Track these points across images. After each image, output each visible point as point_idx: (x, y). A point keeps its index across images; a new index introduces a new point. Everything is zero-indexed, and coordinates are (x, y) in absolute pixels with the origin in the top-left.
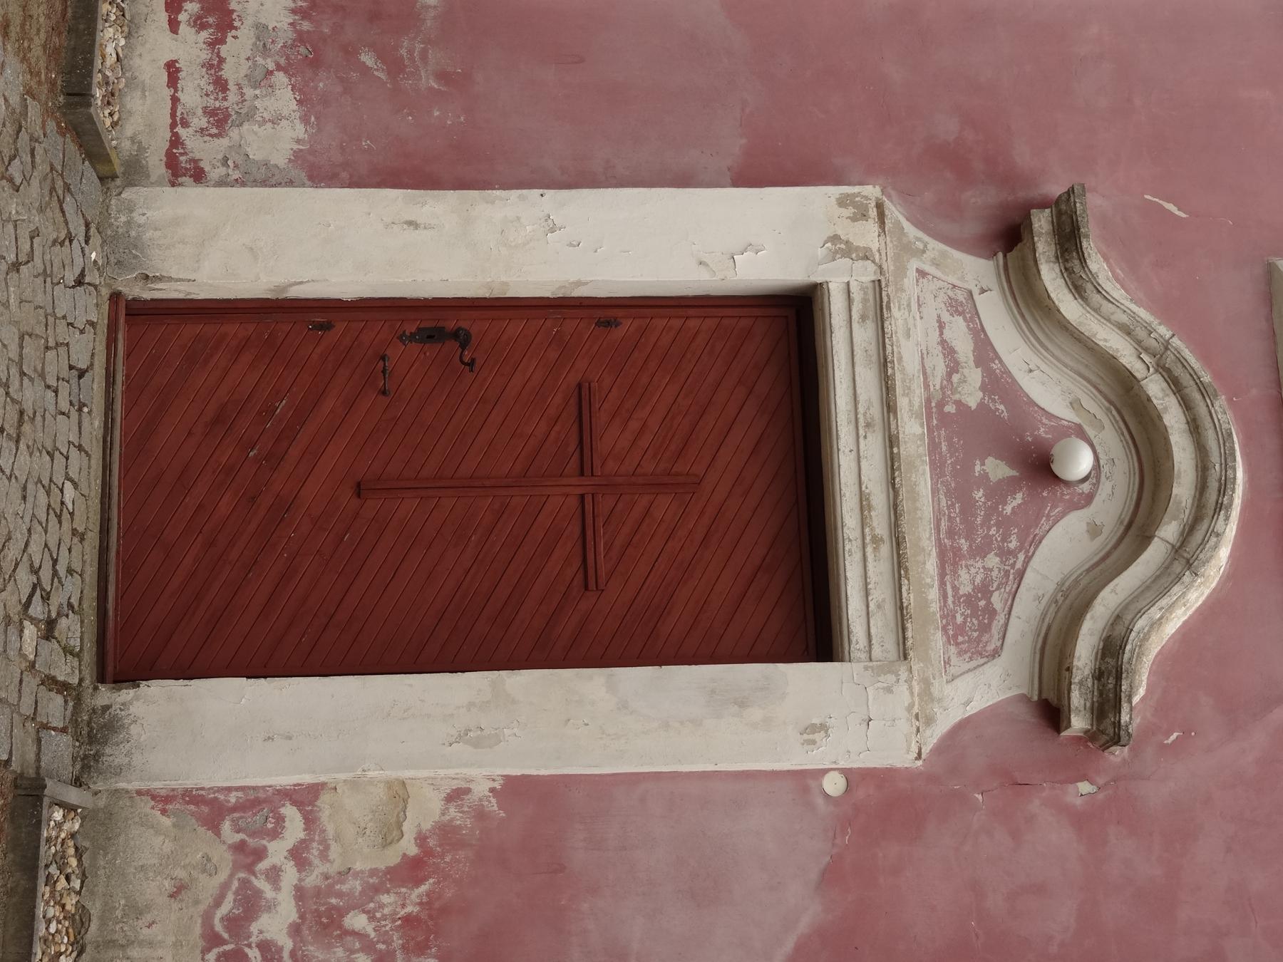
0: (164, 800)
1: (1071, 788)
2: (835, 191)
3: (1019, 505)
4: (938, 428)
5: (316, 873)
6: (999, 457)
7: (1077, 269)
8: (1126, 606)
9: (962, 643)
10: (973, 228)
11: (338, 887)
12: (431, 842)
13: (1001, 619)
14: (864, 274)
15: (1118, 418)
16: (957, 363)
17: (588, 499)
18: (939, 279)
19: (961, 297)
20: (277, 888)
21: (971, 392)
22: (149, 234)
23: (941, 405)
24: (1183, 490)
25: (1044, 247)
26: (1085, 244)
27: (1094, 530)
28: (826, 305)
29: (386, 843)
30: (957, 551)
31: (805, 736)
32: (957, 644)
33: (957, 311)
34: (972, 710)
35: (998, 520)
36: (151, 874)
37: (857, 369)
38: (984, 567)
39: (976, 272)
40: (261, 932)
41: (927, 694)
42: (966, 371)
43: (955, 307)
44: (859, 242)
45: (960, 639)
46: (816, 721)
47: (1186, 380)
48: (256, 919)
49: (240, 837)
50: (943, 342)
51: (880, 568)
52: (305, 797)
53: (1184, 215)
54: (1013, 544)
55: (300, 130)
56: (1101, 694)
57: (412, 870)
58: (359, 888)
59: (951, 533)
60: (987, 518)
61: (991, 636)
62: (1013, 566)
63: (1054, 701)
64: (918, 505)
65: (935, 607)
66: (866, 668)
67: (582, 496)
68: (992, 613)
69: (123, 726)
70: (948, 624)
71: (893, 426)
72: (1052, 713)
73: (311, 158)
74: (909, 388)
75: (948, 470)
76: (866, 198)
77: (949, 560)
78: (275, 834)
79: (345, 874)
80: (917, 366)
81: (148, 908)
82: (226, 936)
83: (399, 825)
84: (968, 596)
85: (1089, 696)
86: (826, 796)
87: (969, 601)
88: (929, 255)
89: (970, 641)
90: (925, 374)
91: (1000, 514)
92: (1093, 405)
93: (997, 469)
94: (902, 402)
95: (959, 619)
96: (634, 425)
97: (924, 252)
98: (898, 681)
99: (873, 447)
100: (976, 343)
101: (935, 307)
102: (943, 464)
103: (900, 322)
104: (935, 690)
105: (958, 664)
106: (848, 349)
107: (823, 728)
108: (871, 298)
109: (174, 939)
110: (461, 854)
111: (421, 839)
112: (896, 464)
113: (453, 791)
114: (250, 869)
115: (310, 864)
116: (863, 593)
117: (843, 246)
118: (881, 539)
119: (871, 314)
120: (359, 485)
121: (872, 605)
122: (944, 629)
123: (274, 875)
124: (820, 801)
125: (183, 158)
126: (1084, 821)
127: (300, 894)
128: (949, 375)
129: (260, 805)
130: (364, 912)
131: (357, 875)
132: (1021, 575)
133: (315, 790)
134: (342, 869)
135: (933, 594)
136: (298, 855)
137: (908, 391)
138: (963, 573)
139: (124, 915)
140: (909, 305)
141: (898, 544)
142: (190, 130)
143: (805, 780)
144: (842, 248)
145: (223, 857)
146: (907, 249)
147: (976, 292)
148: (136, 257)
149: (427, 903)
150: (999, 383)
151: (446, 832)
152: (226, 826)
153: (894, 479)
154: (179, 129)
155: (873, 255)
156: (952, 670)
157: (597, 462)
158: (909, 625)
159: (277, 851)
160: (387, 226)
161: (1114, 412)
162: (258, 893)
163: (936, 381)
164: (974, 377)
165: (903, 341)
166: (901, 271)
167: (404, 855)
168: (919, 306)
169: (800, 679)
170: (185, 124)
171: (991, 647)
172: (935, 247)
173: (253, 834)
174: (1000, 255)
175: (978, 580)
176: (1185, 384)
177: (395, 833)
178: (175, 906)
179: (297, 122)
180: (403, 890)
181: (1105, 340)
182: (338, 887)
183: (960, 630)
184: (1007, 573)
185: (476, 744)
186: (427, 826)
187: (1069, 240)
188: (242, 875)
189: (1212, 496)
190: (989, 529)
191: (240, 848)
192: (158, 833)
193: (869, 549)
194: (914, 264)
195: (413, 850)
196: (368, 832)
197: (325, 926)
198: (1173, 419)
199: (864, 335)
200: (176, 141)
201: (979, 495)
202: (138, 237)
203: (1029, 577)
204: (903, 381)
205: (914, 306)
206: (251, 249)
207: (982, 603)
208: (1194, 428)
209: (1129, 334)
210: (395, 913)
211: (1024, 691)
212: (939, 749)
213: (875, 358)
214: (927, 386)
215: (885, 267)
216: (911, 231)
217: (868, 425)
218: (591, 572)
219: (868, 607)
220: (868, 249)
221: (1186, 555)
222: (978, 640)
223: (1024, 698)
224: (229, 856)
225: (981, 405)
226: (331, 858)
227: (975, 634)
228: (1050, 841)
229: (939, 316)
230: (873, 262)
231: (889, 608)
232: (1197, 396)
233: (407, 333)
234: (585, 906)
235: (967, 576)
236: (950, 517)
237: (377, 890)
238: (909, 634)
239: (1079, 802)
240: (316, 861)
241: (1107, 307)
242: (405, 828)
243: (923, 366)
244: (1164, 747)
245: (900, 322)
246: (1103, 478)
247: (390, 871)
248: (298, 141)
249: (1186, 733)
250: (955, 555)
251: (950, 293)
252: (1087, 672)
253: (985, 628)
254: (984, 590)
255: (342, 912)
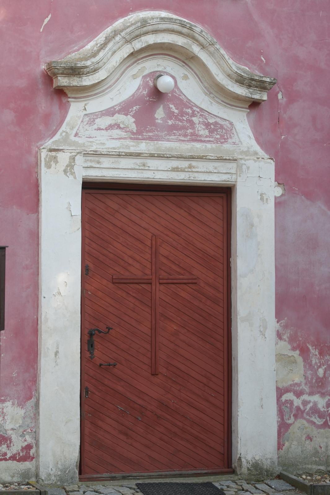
0: (280, 446)
1: (280, 101)
2: (43, 169)
3: (174, 106)
4: (143, 135)
5: (305, 388)
6: (154, 112)
7: (88, 70)
8: (224, 71)
9: (227, 136)
10: (56, 108)
11: (309, 379)
12: (295, 345)
13: (218, 120)
14: (80, 160)
15: (142, 60)
16: (116, 124)
17: (161, 281)
18: (79, 128)
19: (87, 119)
20: (309, 402)
21: (129, 121)
22: (60, 466)
23: (133, 133)
24: (180, 41)
25: (75, 82)
26: (79, 65)
27: (186, 77)
28: (92, 177)
29: (295, 362)
30: (192, 134)
31: (265, 202)
32: (228, 138)
33: (93, 121)
34: (252, 137)
35: (180, 116)
36: (304, 448)
37: (121, 167)
38: (199, 124)
39: (76, 110)
40: (323, 407)
41: (247, 153)
42: (119, 121)
43: (92, 122)
44: (67, 162)
45: (226, 137)
46: (259, 197)
47: (137, 32)
48: (319, 409)
49: (292, 417)
50: (106, 129)
51: (201, 166)
52: (280, 392)
53: (50, 16)
54: (190, 111)
55: (9, 404)
56: (257, 87)
57: (304, 352)
58: (310, 372)
59: (185, 136)
60: (179, 120)
61: (225, 125)
62: (198, 112)
63: (250, 104)
64: (174, 148)
65: (214, 146)
66: (240, 176)
67: (160, 283)
68: (216, 123)
69: (256, 462)
70: (220, 141)
71: (146, 155)
72: (254, 104)
73: (21, 398)
74: (127, 146)
75: (160, 134)
76: (47, 156)
77: (195, 138)
78: (291, 402)
79: (306, 378)
80: (117, 141)
81: (315, 449)
82: (324, 420)
83: (290, 357)
84: (209, 132)
85: (256, 91)
86: (282, 195)
87: (211, 131)
88: (68, 130)
89: (226, 133)
90: (120, 139)
91: (178, 115)
92: (135, 69)
93: (160, 114)
94: (132, 150)
95: (218, 136)
96: (131, 261)
97: (67, 133)
98: (245, 164)
99: (153, 163)
100: (107, 115)
101: (91, 131)
102: (158, 136)
103: (98, 147)
104: (245, 149)
105: (235, 139)
106: (111, 170)
107: (261, 195)
108: (90, 158)
109: (325, 439)
110: (299, 334)
111: (294, 349)
112: (162, 155)
113: (278, 337)
114: (303, 412)
115: (302, 390)
116: (210, 174)
117: (69, 168)
118: (190, 165)
119: (97, 159)
120: (152, 375)
121: (215, 171)
122: (222, 143)
123: (305, 403)
124: (283, 198)
125: (21, 454)
126: (292, 98)
127: (311, 394)
128: (120, 128)
129: (283, 408)
130: (318, 370)
131: (305, 373)
132: (202, 110)
133: (278, 389)
134: (304, 378)
135: (209, 146)
136: (298, 394)
137: (128, 147)
138: (201, 133)
139: (318, 457)
140: (91, 142)
141: (193, 158)
142: (8, 452)
143: (279, 204)
144: (69, 169)
145: (300, 422)
146: (66, 140)
147: (85, 112)
148: (69, 472)
149: (315, 347)
150: (124, 108)
151: (292, 340)
152: (290, 422)
153: (167, 157)
154: (8, 457)
155: (73, 156)
156: (237, 142)
157: (146, 277)
158: (224, 158)
159: (297, 402)
160: (57, 365)
161: (140, 61)
162: (311, 408)
163: (123, 134)
164: (120, 118)
165: (106, 146)
166: (75, 144)
167: (299, 355)
168: (90, 137)
169: (243, 202)
170: (5, 454)
171: (229, 126)
172: (64, 127)
173: (291, 411)
174: (70, 100)
175: (204, 127)
176: (139, 33)
177: (292, 358)
178: (314, 439)
179: (4, 405)
180: (311, 355)
181: (116, 62)
182: (309, 379)
183: (222, 137)
184: (201, 115)
185: (266, 328)
186: (289, 347)
187: (74, 71)
188: (305, 415)
189: (185, 30)
190: (184, 120)
191: (296, 416)
192: (291, 447)
193: (194, 170)
194: (72, 138)
195: (298, 352)
196: (291, 369)
197: (322, 384)
198: (151, 39)
199: (106, 162)
200: (13, 458)
201: (170, 123)
202: (61, 471)
203: (203, 106)
204: (123, 148)
205: (91, 140)
206: (66, 422)
207: (212, 126)
208: (155, 32)
209: (115, 52)
210: (318, 358)
211: (245, 114)
212: (267, 151)
213: (116, 159)
214: (125, 138)
215: (78, 151)
216: (57, 137)
217: (144, 165)
218: (190, 281)
219: (215, 173)
220: (70, 157)
221: (207, 45)
222: (226, 130)
223: (248, 115)
224: (299, 420)
225: (133, 116)
226: (300, 382)
227: (224, 131)
228: (297, 112)
229: (95, 129)
230: (76, 156)
231: (217, 164)
232: (145, 29)
233: (90, 355)
234: (317, 288)
235: (202, 131)
236: (179, 135)
237: (311, 365)
238: (228, 158)
239: (285, 99)
240: (301, 388)
241: (104, 60)
242: (290, 355)
243: (116, 139)
244: (267, 63)
245: (98, 147)
246: (165, 70)
247: (304, 360)
248: (13, 404)
249: (262, 54)
250: (193, 135)
251: (85, 123)
252: (247, 91)
253: (222, 127)
254: (207, 125)
255: (318, 378)
